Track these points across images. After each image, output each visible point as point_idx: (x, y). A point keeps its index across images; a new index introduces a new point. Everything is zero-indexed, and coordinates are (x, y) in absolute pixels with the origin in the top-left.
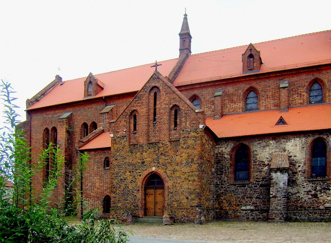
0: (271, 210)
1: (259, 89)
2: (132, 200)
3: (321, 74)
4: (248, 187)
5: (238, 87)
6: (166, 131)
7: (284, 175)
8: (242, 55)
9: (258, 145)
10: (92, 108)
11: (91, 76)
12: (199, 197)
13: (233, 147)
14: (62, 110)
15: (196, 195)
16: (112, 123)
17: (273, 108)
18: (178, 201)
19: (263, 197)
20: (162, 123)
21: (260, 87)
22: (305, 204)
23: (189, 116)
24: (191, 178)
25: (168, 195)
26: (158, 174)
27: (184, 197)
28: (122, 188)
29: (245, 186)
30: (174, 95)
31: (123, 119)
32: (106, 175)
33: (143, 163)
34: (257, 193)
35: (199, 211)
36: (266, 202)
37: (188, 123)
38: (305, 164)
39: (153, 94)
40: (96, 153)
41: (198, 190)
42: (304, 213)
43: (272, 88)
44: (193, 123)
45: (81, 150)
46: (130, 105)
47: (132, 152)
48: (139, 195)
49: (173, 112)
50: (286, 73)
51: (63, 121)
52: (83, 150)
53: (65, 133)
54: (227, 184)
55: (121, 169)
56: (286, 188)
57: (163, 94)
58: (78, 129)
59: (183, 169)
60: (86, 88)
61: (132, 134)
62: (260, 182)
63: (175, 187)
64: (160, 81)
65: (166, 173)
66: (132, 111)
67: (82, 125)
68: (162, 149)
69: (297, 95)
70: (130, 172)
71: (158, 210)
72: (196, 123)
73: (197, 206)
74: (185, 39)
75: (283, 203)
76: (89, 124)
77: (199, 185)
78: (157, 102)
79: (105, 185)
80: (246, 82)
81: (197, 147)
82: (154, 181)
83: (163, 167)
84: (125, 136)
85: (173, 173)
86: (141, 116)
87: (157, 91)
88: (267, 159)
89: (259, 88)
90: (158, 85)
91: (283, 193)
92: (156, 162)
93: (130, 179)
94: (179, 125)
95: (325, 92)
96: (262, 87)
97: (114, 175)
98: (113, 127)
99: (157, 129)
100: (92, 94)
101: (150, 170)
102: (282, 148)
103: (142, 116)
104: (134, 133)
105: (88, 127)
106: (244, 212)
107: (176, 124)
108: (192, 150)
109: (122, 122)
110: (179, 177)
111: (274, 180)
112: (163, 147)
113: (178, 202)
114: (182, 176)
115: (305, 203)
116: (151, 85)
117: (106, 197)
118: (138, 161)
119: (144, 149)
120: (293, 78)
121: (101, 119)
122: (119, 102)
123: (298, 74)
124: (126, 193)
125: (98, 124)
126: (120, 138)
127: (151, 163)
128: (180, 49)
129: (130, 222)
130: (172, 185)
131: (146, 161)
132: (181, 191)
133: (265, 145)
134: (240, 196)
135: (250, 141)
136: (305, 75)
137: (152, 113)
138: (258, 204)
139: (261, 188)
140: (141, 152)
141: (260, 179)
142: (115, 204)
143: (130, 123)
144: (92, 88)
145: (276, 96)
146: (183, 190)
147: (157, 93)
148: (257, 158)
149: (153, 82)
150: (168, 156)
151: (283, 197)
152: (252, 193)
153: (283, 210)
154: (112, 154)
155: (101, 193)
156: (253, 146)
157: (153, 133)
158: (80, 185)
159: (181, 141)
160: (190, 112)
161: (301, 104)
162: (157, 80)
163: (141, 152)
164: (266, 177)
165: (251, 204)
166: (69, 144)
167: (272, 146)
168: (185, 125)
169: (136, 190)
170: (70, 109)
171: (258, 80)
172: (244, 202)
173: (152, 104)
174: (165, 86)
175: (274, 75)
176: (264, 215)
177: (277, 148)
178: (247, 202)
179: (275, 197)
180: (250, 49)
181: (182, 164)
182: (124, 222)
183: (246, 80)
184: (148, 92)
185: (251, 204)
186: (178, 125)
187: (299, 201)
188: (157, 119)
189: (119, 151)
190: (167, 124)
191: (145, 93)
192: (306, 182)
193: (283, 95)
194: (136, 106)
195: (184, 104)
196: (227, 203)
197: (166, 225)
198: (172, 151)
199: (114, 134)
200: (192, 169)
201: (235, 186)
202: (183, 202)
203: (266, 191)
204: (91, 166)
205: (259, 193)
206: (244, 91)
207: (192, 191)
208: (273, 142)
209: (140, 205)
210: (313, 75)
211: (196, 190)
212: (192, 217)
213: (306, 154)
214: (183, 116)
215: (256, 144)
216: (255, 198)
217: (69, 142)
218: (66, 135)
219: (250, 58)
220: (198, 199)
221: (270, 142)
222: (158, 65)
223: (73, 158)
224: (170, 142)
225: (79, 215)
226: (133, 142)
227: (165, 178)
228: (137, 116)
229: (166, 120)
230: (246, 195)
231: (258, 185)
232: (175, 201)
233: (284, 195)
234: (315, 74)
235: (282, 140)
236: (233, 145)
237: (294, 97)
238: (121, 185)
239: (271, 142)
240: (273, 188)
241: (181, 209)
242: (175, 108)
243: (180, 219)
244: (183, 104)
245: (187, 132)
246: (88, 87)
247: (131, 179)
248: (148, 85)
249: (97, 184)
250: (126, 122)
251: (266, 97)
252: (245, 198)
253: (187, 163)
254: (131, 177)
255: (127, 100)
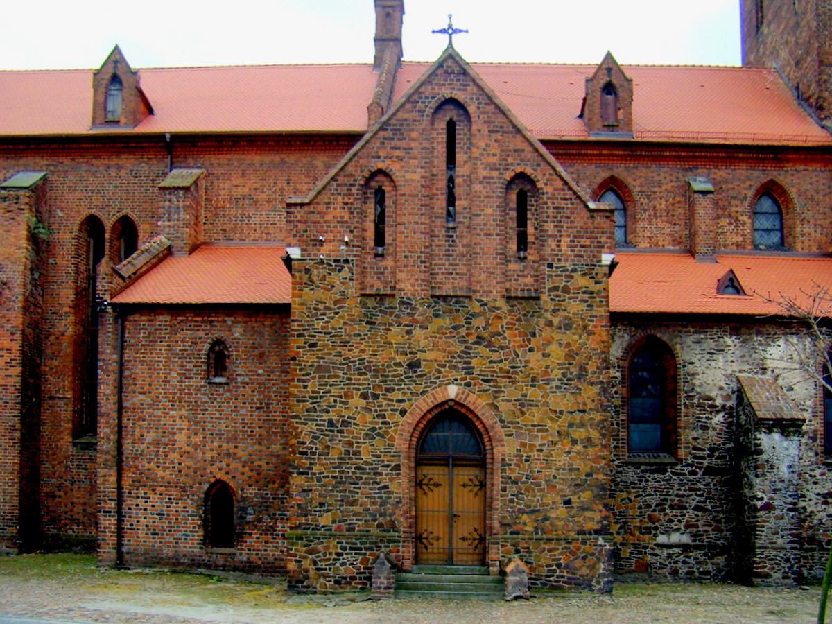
0: (760, 548)
1: (635, 186)
2: (374, 503)
3: (783, 173)
4: (674, 474)
5: (578, 170)
6: (495, 262)
7: (791, 442)
8: (587, 81)
9: (694, 345)
10: (119, 168)
11: (118, 57)
12: (605, 501)
13: (628, 346)
14: (8, 158)
15: (596, 491)
16: (295, 205)
17: (671, 248)
18: (539, 510)
19: (712, 507)
20: (479, 232)
21: (635, 180)
22: (821, 531)
23: (568, 218)
24: (579, 434)
25: (504, 489)
26: (463, 411)
27: (558, 499)
28: (334, 455)
29: (664, 472)
30: (517, 139)
31: (340, 198)
32: (215, 404)
33: (414, 365)
34: (698, 493)
35: (608, 547)
36: (721, 523)
37: (565, 241)
38: (815, 414)
39: (445, 126)
40: (175, 322)
41: (601, 477)
42: (820, 558)
43: (666, 190)
44: (582, 243)
45: (121, 304)
46: (364, 150)
47: (374, 323)
48: (400, 484)
49: (514, 197)
50: (703, 154)
51: (17, 198)
52: (127, 304)
53: (24, 243)
54: (616, 463)
55: (331, 381)
56: (795, 482)
57: (479, 131)
58: (67, 237)
59: (551, 399)
60: (101, 98)
61: (369, 257)
62: (704, 458)
63: (527, 461)
64: (469, 85)
65: (496, 408)
66: (370, 171)
67: (82, 224)
68: (479, 322)
69: (728, 221)
70: (364, 396)
71: (460, 541)
72: (590, 246)
73: (598, 532)
74: (390, 10)
75: (789, 526)
76: (109, 223)
77: (604, 459)
78: (457, 155)
79: (212, 442)
80: (600, 160)
81: (595, 326)
82: (452, 438)
83: (485, 386)
84: (347, 261)
85: (518, 413)
86: (404, 195)
87: (455, 118)
88: (720, 392)
89: (634, 183)
90: (463, 97)
91: (790, 496)
92: (460, 366)
93: (365, 421)
94: (534, 243)
95: (791, 221)
96: (641, 183)
97: (301, 404)
98: (299, 221)
99: (460, 249)
100: (123, 120)
101: (441, 395)
102: (756, 362)
103: (410, 195)
104: (377, 255)
105: (103, 230)
106: (665, 552)
107: (522, 242)
108: (580, 337)
109: (334, 209)
110: (541, 428)
111: (764, 457)
112: (483, 314)
113: (537, 514)
114: (549, 424)
115: (819, 530)
116: (436, 90)
117: (212, 485)
118: (394, 358)
119: (415, 317)
120: (717, 171)
121: (164, 208)
122: (219, 162)
123: (731, 163)
124: (347, 476)
125: (143, 229)
126: (329, 265)
127: (443, 370)
128: (378, 37)
129: (385, 588)
130: (515, 453)
131: (424, 360)
132: (546, 476)
133: (713, 347)
134: (654, 500)
135: (674, 331)
136: (745, 168)
137: (442, 189)
138: (700, 529)
139: (708, 479)
140: (406, 325)
141: (704, 450)
142: (306, 515)
143: (363, 214)
144: (120, 99)
145: (677, 213)
146: (553, 472)
147: (457, 123)
148: (694, 385)
149: (444, 85)
150: (502, 348)
151: (789, 510)
152: (686, 493)
153: (792, 548)
154: (296, 323)
155: (195, 472)
156: (682, 348)
157: (447, 263)
158: (114, 437)
159: (545, 302)
160: (569, 206)
161: (738, 246)
162: (459, 80)
163: (406, 325)
164: (719, 445)
165: (683, 528)
166: (35, 286)
167: (730, 352)
168: (556, 248)
169: (388, 466)
170: (38, 160)
171: (631, 160)
172: (664, 519)
173: (441, 158)
174: (486, 104)
175: (674, 153)
176: (719, 561)
177: (745, 359)
178: (670, 521)
179: (768, 507)
180: (607, 66)
181: (548, 382)
182: (341, 588)
183: (600, 155)
184: (428, 116)
185: (682, 526)
186: (529, 245)
187: (804, 521)
188: (461, 213)
189: (324, 314)
190: (497, 235)
191: (416, 115)
192: (819, 468)
193: (701, 212)
194: (385, 158)
195: (551, 175)
196: (618, 523)
197: (516, 598)
198: (517, 332)
199: (303, 250)
200: (580, 400)
201: (638, 468)
202: (552, 515)
203: (721, 490)
204: (155, 369)
205: (701, 495)
206: (595, 186)
207: (584, 477)
208: (733, 341)
209: (403, 523)
210: (764, 171)
211: (595, 476)
212: (585, 571)
213: (816, 385)
214: (548, 217)
215: (691, 343)
216: (693, 509)
217: (36, 276)
218: (27, 248)
219: (607, 94)
220: (601, 507)
221: (726, 339)
222: (455, 31)
223: (47, 338)
224: (509, 298)
225: (108, 550)
226: (372, 286)
227: (493, 427)
228: (387, 195)
229: (492, 222)
230: (669, 498)
231: (700, 468)
232: (527, 513)
233: (790, 504)
234: (769, 168)
235: (755, 339)
236: (627, 337)
237: (721, 224)
238: (329, 443)
239: (729, 340)
240: (763, 481)
241: (550, 540)
242: (520, 187)
243: (547, 576)
244: (547, 176)
245: (564, 274)
246: (106, 93)
247: (370, 423)
248: (427, 90)
249: (181, 438)
250: (350, 208)
251: (653, 213)
252: (667, 507)
253: (566, 380)
254: (369, 418)
255: (244, 157)
